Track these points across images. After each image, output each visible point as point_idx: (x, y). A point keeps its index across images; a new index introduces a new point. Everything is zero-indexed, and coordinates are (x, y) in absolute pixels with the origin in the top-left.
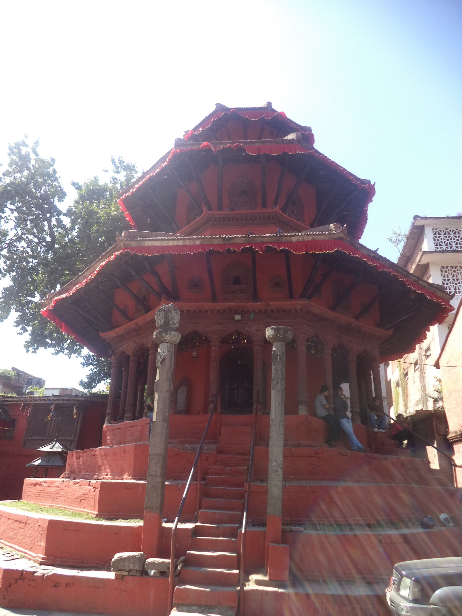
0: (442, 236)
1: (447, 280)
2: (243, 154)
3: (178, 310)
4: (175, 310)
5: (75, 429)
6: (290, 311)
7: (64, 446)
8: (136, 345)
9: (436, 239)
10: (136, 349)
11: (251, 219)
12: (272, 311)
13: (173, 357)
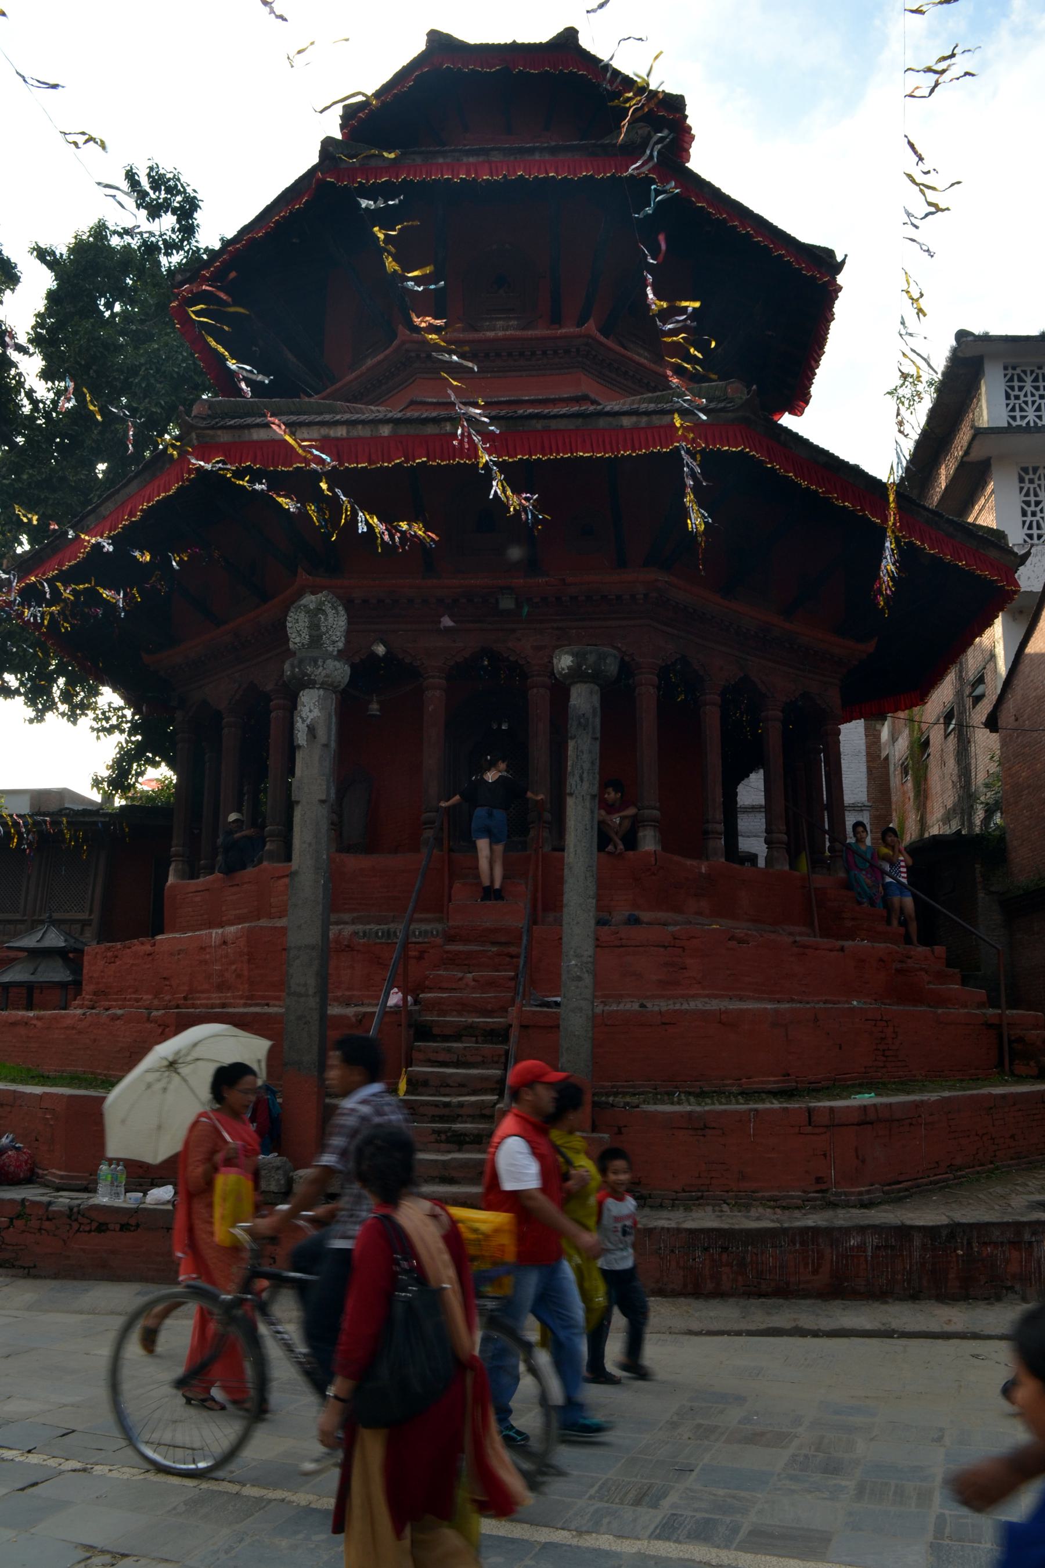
0: (1028, 387)
1: (1033, 504)
3: (340, 608)
4: (334, 608)
5: (90, 892)
7: (68, 934)
9: (1012, 394)
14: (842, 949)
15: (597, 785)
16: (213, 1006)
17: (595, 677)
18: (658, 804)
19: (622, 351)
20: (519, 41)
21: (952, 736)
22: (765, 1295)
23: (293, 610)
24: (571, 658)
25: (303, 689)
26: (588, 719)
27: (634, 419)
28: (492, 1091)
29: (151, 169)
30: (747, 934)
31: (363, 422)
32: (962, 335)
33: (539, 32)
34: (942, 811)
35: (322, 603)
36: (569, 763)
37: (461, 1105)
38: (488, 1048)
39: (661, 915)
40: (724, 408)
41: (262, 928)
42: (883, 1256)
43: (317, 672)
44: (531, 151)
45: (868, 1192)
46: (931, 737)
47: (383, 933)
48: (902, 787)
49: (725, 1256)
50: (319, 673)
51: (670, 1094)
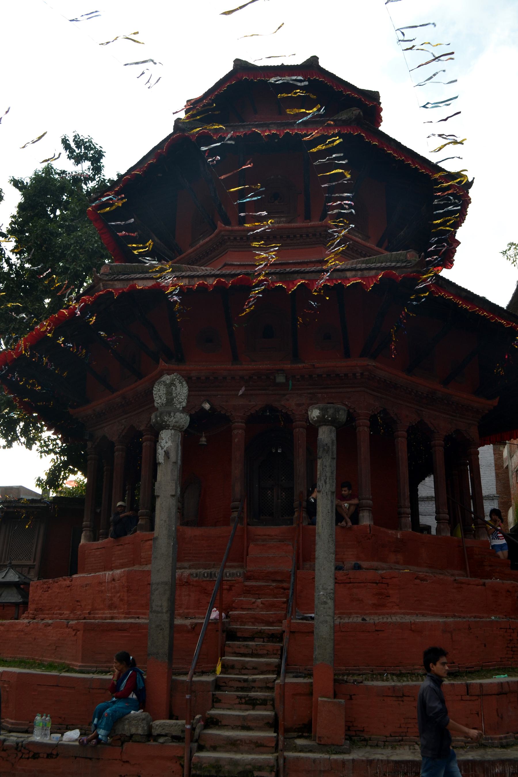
2: (276, 141)
3: (184, 383)
4: (180, 382)
8: (123, 427)
11: (288, 237)
13: (180, 448)
14: (484, 584)
17: (333, 422)
23: (157, 384)
24: (318, 411)
25: (163, 430)
26: (329, 447)
28: (273, 672)
30: (426, 576)
31: (198, 277)
35: (173, 380)
36: (318, 473)
37: (254, 681)
38: (270, 646)
39: (375, 564)
40: (406, 266)
45: (506, 738)
47: (208, 574)
50: (172, 420)
51: (381, 675)
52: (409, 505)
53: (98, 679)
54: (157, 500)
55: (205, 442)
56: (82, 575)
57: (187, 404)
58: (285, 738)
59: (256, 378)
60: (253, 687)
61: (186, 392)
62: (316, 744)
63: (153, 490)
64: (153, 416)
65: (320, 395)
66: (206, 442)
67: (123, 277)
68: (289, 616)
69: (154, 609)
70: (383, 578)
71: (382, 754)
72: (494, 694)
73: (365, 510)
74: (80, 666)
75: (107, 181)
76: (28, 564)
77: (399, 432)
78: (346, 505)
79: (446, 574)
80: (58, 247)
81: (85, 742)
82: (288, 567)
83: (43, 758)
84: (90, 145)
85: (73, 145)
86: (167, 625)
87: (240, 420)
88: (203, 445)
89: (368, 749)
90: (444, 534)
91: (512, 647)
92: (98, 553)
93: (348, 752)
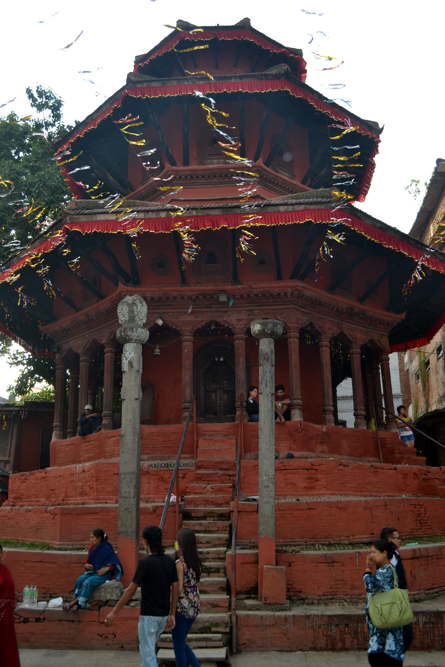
3: (144, 303)
4: (141, 303)
5: (9, 446)
6: (279, 294)
8: (87, 341)
10: (87, 347)
12: (256, 295)
14: (395, 469)
15: (274, 389)
16: (78, 504)
17: (272, 335)
18: (301, 397)
19: (275, 173)
20: (221, 24)
21: (441, 359)
22: (322, 649)
23: (120, 303)
24: (260, 326)
25: (126, 343)
26: (269, 356)
27: (286, 207)
28: (223, 545)
29: (38, 87)
30: (348, 462)
31: (152, 211)
32: (439, 161)
33: (231, 20)
34: (437, 397)
35: (135, 300)
36: (260, 378)
37: (208, 553)
38: (221, 523)
39: (305, 453)
40: (330, 201)
41: (103, 464)
42: (428, 628)
43: (133, 334)
44: (230, 78)
45: (418, 594)
46: (430, 360)
47: (165, 465)
48: (416, 385)
49: (347, 630)
50: (134, 335)
51: (314, 545)
52: (332, 403)
53: (76, 555)
54: (123, 403)
55: (159, 352)
56: (55, 468)
57: (147, 321)
58: (236, 600)
59: (202, 297)
60: (207, 558)
61: (145, 310)
62: (262, 603)
63: (119, 396)
64: (118, 332)
65: (257, 311)
66: (160, 353)
67: (87, 212)
68: (236, 498)
69: (122, 495)
70: (312, 465)
71: (318, 610)
72: (409, 559)
73: (296, 408)
74: (58, 545)
75: (65, 127)
76: (4, 459)
77: (323, 343)
78: (280, 404)
79: (364, 460)
80: (24, 185)
81: (68, 608)
82: (231, 458)
83: (32, 622)
84: (50, 95)
85: (36, 95)
86: (134, 508)
87: (189, 334)
88: (158, 355)
89: (305, 606)
90: (361, 428)
91: (420, 520)
92: (68, 449)
93: (289, 609)
